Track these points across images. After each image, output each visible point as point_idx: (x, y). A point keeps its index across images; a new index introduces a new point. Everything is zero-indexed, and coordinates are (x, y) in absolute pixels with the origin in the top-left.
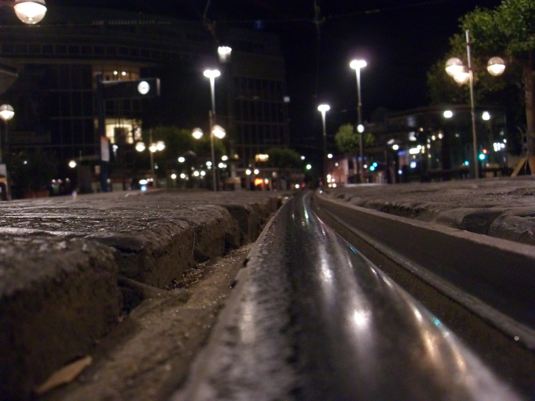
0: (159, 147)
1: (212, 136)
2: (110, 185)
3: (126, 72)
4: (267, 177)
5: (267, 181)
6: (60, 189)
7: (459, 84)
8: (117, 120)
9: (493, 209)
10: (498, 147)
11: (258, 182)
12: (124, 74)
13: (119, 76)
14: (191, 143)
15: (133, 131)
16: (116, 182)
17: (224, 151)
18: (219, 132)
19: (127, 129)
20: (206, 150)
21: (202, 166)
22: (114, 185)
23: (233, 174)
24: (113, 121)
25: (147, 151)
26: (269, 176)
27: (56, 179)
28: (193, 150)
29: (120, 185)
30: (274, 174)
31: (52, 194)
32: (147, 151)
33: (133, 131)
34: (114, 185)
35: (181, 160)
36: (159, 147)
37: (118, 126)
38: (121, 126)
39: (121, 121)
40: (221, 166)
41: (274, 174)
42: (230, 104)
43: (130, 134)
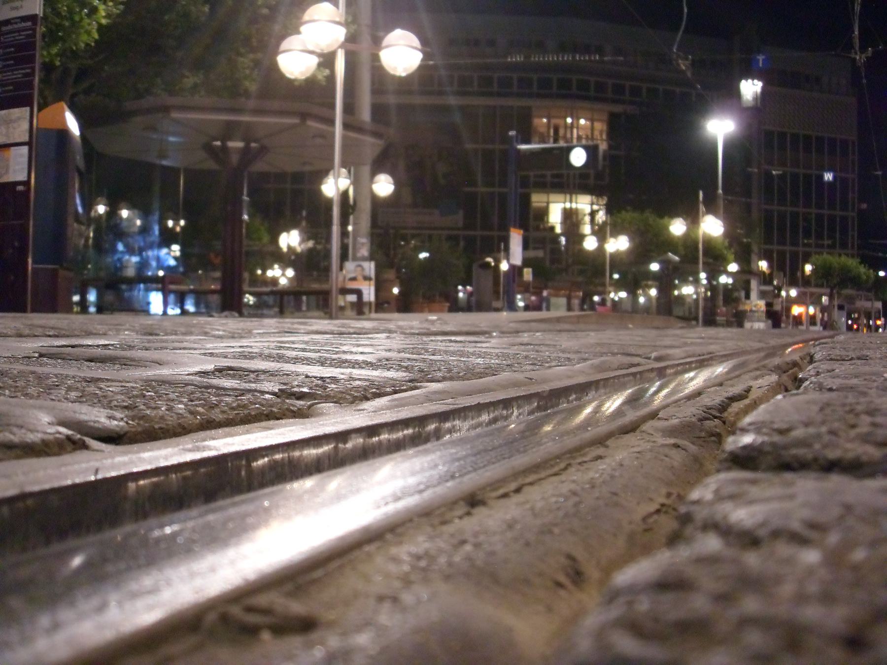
0: (619, 244)
1: (701, 232)
2: (547, 300)
3: (586, 119)
4: (813, 303)
5: (811, 310)
6: (469, 300)
7: (716, 238)
8: (568, 196)
9: (672, 441)
10: (879, 322)
11: (796, 310)
12: (582, 122)
13: (575, 125)
14: (670, 244)
15: (593, 214)
16: (557, 296)
17: (731, 257)
18: (712, 227)
19: (583, 210)
20: (695, 256)
21: (691, 279)
22: (553, 300)
23: (754, 295)
24: (561, 197)
25: (600, 249)
26: (816, 302)
27: (464, 286)
28: (675, 253)
29: (859, 260)
30: (824, 299)
31: (455, 307)
32: (600, 249)
33: (593, 214)
34: (553, 300)
35: (655, 267)
36: (619, 244)
37: (568, 205)
38: (574, 206)
39: (574, 197)
40: (724, 279)
41: (824, 299)
42: (744, 183)
43: (587, 219)
